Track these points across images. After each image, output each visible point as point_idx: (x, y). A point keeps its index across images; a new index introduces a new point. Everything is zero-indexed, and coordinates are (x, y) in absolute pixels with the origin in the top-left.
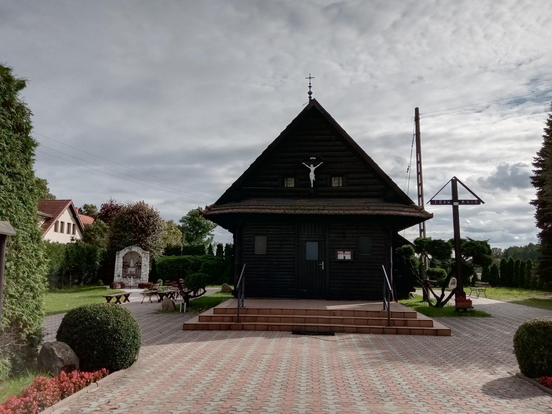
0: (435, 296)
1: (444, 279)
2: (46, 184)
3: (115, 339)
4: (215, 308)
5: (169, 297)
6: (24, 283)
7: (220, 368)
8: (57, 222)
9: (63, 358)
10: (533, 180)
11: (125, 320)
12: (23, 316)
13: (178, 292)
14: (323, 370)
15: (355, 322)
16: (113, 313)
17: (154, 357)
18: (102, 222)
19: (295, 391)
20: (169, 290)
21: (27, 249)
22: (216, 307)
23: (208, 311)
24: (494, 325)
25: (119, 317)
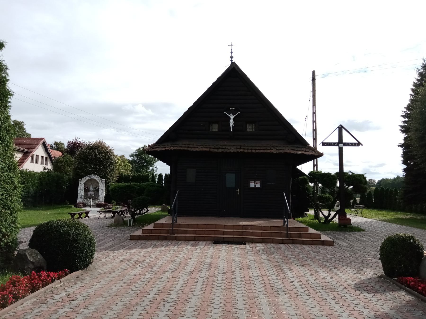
0: (323, 216)
1: (330, 202)
2: (24, 125)
3: (76, 248)
4: (155, 223)
5: (120, 214)
6: (3, 203)
7: (156, 270)
8: (33, 155)
9: (34, 261)
10: (401, 128)
11: (83, 233)
12: (2, 228)
13: (127, 211)
14: (235, 271)
15: (262, 234)
16: (73, 227)
17: (106, 260)
18: (69, 156)
19: (213, 287)
20: (120, 209)
21: (5, 176)
22: (157, 222)
23: (149, 225)
24: (366, 238)
25: (78, 230)
